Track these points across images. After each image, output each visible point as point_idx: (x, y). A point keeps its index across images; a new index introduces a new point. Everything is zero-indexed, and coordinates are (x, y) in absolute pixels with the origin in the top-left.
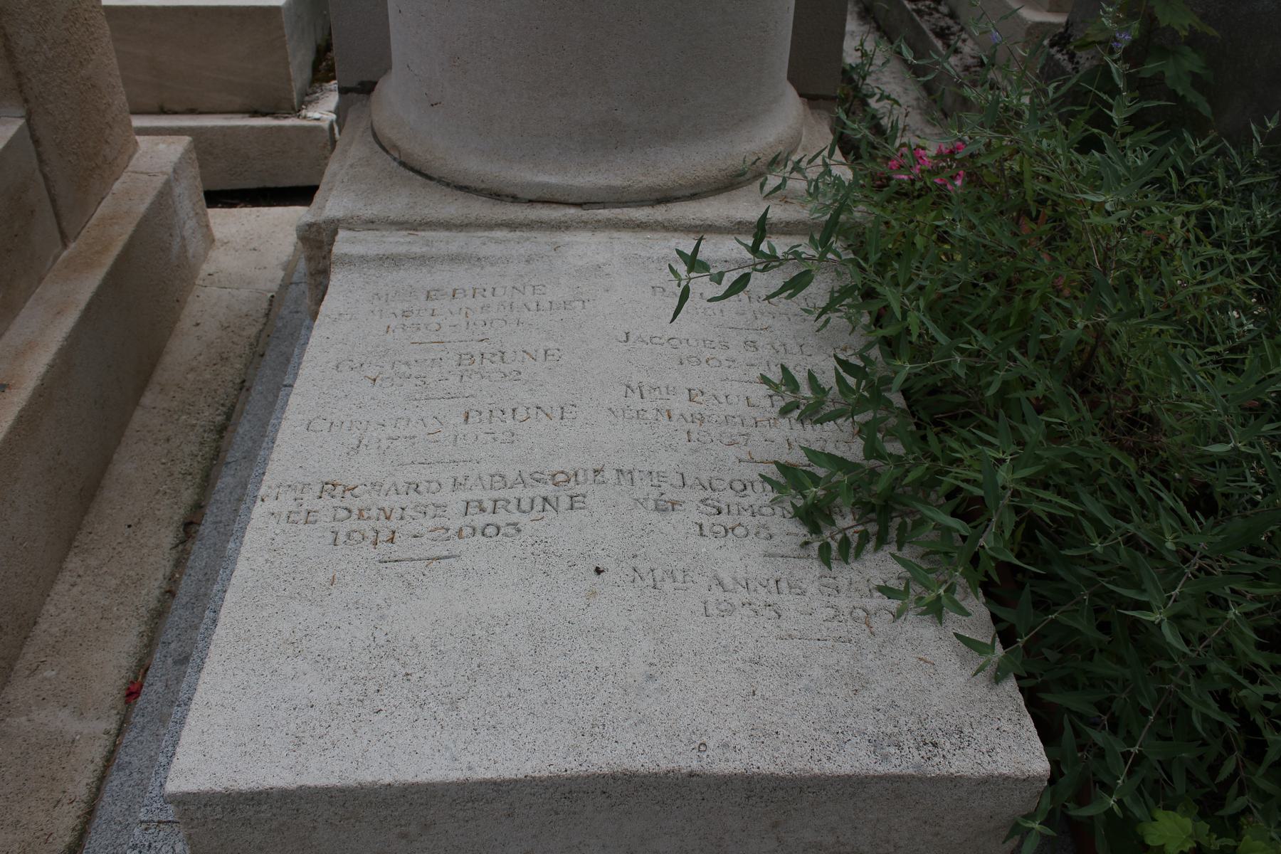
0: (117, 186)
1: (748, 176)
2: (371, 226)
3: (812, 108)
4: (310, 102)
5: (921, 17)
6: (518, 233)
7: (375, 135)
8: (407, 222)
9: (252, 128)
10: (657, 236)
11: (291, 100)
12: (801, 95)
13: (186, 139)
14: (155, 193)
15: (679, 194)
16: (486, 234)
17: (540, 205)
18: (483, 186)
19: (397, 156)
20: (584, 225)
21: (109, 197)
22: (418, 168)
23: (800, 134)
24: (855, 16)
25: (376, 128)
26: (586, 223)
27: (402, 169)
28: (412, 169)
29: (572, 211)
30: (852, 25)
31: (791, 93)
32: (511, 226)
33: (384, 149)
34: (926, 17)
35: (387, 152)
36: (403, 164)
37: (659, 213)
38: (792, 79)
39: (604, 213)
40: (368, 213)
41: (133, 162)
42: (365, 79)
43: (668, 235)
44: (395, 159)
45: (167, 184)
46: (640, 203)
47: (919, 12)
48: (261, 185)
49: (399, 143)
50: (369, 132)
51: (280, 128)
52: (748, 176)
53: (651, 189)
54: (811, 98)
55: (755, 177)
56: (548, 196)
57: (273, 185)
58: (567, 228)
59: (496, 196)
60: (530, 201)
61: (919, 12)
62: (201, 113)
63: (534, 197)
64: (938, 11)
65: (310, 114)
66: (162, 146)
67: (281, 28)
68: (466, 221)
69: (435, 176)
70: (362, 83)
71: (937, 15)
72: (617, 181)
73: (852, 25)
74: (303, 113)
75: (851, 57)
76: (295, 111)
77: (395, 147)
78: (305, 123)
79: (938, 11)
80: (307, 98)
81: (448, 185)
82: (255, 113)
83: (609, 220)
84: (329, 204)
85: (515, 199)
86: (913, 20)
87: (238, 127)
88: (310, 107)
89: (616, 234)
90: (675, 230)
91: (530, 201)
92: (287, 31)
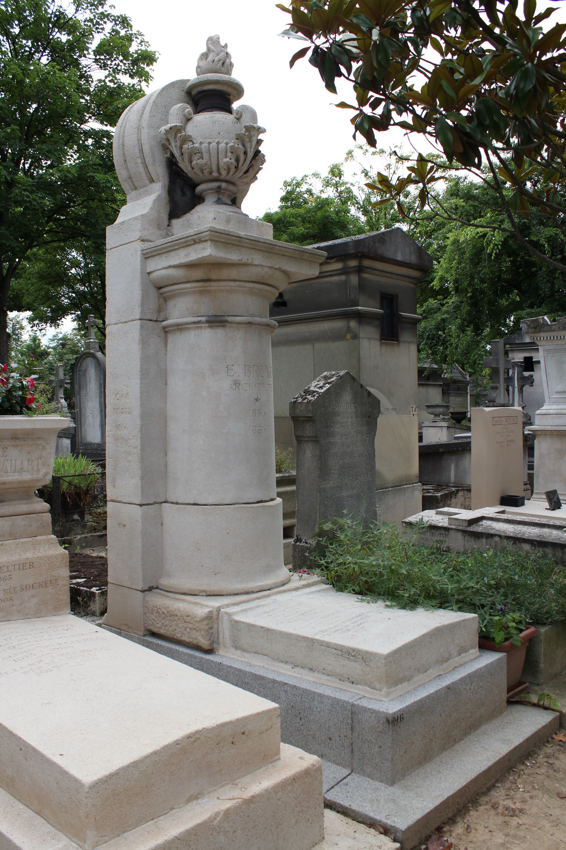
19: (204, 594)
46: (277, 587)
56: (261, 589)
59: (247, 593)
70: (149, 588)
72: (275, 581)
81: (230, 595)
85: (253, 592)
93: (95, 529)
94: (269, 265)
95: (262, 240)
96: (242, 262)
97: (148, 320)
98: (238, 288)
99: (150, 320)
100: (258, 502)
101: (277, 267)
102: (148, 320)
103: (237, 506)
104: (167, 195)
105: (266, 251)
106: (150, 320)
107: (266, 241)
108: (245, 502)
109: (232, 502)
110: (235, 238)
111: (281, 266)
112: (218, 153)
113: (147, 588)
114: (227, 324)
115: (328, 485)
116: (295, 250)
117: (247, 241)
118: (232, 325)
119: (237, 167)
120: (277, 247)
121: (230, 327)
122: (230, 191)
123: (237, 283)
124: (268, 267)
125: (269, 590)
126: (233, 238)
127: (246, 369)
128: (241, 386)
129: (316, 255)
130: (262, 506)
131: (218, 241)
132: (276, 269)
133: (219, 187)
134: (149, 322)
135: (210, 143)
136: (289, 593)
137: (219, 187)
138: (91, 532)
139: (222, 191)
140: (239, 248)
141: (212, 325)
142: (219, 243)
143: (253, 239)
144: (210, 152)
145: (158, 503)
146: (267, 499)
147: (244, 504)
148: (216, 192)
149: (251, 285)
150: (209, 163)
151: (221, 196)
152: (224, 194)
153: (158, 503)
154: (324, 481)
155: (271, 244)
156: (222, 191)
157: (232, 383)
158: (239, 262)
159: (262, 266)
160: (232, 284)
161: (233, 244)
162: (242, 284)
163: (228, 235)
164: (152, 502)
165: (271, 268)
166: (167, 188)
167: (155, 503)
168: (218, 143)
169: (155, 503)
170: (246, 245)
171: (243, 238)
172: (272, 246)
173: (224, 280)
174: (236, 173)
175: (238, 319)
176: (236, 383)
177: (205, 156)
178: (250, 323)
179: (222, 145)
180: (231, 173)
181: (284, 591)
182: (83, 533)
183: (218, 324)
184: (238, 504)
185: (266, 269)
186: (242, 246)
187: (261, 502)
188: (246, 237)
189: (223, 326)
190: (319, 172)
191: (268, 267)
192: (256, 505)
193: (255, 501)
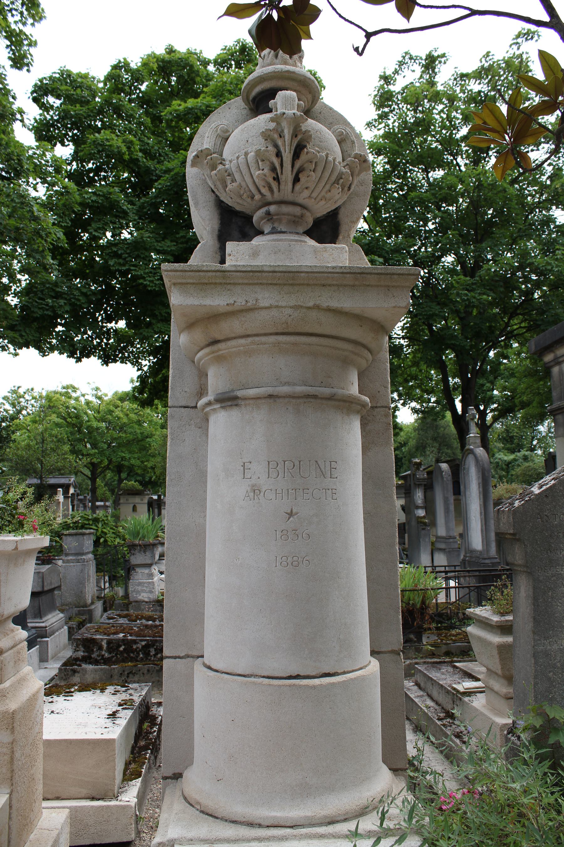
0: (32, 837)
1: (370, 808)
2: (191, 842)
3: (395, 775)
4: (122, 792)
5: (446, 728)
6: (263, 843)
7: (185, 798)
8: (208, 840)
9: (92, 807)
10: (330, 841)
11: (113, 790)
12: (390, 769)
13: (68, 810)
14: (53, 840)
15: (339, 819)
16: (247, 844)
17: (272, 828)
18: (244, 820)
19: (199, 807)
20: (295, 837)
21: (28, 843)
22: (210, 813)
23: (392, 786)
24: (411, 731)
25: (186, 795)
26: (295, 836)
27: (201, 814)
28: (207, 814)
29: (289, 830)
30: (410, 736)
31: (385, 769)
32: (259, 839)
33: (191, 805)
34: (449, 728)
35: (193, 806)
36: (202, 812)
37: (330, 829)
38: (384, 761)
39: (304, 831)
40: (190, 835)
41: (40, 823)
42: (176, 772)
43: (336, 840)
44: (197, 810)
45: (58, 835)
46: (321, 824)
47: (444, 725)
48: (92, 843)
49: (201, 801)
50: (182, 798)
51: (108, 806)
52: (370, 808)
53: (326, 817)
54: (395, 770)
55: (374, 809)
56: (276, 823)
57: (99, 842)
58: (287, 839)
59: (251, 824)
60: (268, 826)
61: (444, 725)
62: (62, 799)
63: (269, 824)
64: (454, 724)
65: (123, 799)
66: (54, 815)
67: (114, 750)
68: (238, 838)
69: (220, 816)
70: (174, 774)
71: (454, 726)
72: (309, 814)
73: (410, 736)
74: (119, 798)
75: (411, 752)
76: (116, 797)
77: (199, 803)
78: (121, 803)
79: (454, 724)
80: (122, 789)
81: (226, 821)
82: (93, 799)
83: (307, 834)
84: (169, 832)
85: (260, 826)
86: (442, 730)
87: (85, 806)
88: (122, 795)
89: (310, 842)
90: (339, 838)
91: (268, 826)
92: (116, 752)
93: (434, 654)
94: (292, 303)
95: (266, 269)
96: (237, 307)
97: (181, 407)
98: (255, 347)
99: (185, 407)
100: (290, 677)
101: (311, 304)
102: (181, 407)
103: (252, 679)
104: (216, 242)
105: (285, 285)
106: (185, 407)
107: (277, 269)
108: (266, 674)
109: (247, 673)
110: (214, 274)
111: (318, 302)
112: (249, 167)
113: (170, 774)
114: (240, 402)
115: (555, 647)
116: (342, 273)
117: (238, 274)
118: (247, 402)
119: (277, 179)
120: (302, 275)
121: (246, 405)
122: (288, 214)
123: (250, 340)
124: (291, 307)
125: (291, 827)
126: (210, 274)
127: (271, 466)
128: (262, 494)
129: (393, 274)
130: (290, 686)
131: (187, 284)
132: (309, 308)
133: (268, 213)
134: (182, 409)
135: (238, 158)
136: (333, 840)
137: (268, 213)
138: (426, 657)
139: (274, 217)
140: (229, 287)
141: (223, 405)
142: (189, 286)
143: (249, 269)
144: (240, 170)
145: (193, 657)
146: (313, 674)
147: (264, 677)
148: (268, 220)
149: (272, 339)
150: (243, 184)
151: (276, 225)
152: (280, 221)
153: (193, 657)
154: (546, 638)
155: (289, 272)
156: (274, 217)
157: (249, 489)
158: (230, 309)
159: (277, 307)
160: (242, 341)
161: (216, 283)
162: (257, 339)
163: (199, 271)
164: (182, 655)
165: (296, 307)
166: (216, 232)
167: (187, 656)
168: (246, 154)
169: (187, 656)
170: (240, 281)
171: (229, 271)
172: (291, 275)
173: (235, 338)
174: (282, 187)
175: (252, 392)
176: (255, 490)
177: (237, 176)
178: (270, 396)
179: (251, 155)
180: (275, 189)
181: (322, 836)
182: (416, 658)
183: (229, 403)
184: (256, 676)
185: (290, 311)
186: (235, 284)
187: (298, 677)
188: (233, 269)
189: (236, 405)
190: (25, 109)
191: (291, 307)
192: (266, 681)
193: (285, 675)
